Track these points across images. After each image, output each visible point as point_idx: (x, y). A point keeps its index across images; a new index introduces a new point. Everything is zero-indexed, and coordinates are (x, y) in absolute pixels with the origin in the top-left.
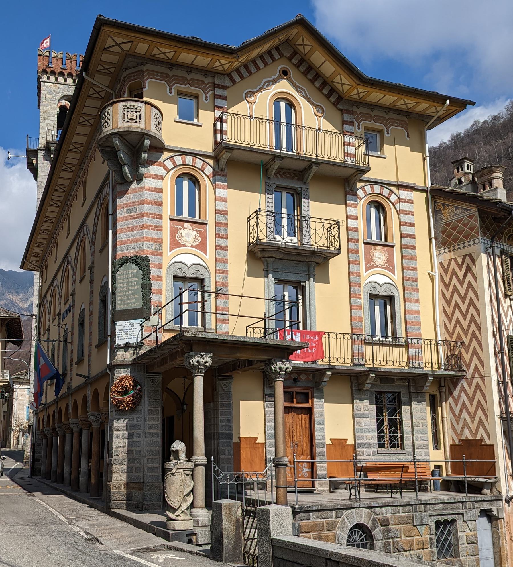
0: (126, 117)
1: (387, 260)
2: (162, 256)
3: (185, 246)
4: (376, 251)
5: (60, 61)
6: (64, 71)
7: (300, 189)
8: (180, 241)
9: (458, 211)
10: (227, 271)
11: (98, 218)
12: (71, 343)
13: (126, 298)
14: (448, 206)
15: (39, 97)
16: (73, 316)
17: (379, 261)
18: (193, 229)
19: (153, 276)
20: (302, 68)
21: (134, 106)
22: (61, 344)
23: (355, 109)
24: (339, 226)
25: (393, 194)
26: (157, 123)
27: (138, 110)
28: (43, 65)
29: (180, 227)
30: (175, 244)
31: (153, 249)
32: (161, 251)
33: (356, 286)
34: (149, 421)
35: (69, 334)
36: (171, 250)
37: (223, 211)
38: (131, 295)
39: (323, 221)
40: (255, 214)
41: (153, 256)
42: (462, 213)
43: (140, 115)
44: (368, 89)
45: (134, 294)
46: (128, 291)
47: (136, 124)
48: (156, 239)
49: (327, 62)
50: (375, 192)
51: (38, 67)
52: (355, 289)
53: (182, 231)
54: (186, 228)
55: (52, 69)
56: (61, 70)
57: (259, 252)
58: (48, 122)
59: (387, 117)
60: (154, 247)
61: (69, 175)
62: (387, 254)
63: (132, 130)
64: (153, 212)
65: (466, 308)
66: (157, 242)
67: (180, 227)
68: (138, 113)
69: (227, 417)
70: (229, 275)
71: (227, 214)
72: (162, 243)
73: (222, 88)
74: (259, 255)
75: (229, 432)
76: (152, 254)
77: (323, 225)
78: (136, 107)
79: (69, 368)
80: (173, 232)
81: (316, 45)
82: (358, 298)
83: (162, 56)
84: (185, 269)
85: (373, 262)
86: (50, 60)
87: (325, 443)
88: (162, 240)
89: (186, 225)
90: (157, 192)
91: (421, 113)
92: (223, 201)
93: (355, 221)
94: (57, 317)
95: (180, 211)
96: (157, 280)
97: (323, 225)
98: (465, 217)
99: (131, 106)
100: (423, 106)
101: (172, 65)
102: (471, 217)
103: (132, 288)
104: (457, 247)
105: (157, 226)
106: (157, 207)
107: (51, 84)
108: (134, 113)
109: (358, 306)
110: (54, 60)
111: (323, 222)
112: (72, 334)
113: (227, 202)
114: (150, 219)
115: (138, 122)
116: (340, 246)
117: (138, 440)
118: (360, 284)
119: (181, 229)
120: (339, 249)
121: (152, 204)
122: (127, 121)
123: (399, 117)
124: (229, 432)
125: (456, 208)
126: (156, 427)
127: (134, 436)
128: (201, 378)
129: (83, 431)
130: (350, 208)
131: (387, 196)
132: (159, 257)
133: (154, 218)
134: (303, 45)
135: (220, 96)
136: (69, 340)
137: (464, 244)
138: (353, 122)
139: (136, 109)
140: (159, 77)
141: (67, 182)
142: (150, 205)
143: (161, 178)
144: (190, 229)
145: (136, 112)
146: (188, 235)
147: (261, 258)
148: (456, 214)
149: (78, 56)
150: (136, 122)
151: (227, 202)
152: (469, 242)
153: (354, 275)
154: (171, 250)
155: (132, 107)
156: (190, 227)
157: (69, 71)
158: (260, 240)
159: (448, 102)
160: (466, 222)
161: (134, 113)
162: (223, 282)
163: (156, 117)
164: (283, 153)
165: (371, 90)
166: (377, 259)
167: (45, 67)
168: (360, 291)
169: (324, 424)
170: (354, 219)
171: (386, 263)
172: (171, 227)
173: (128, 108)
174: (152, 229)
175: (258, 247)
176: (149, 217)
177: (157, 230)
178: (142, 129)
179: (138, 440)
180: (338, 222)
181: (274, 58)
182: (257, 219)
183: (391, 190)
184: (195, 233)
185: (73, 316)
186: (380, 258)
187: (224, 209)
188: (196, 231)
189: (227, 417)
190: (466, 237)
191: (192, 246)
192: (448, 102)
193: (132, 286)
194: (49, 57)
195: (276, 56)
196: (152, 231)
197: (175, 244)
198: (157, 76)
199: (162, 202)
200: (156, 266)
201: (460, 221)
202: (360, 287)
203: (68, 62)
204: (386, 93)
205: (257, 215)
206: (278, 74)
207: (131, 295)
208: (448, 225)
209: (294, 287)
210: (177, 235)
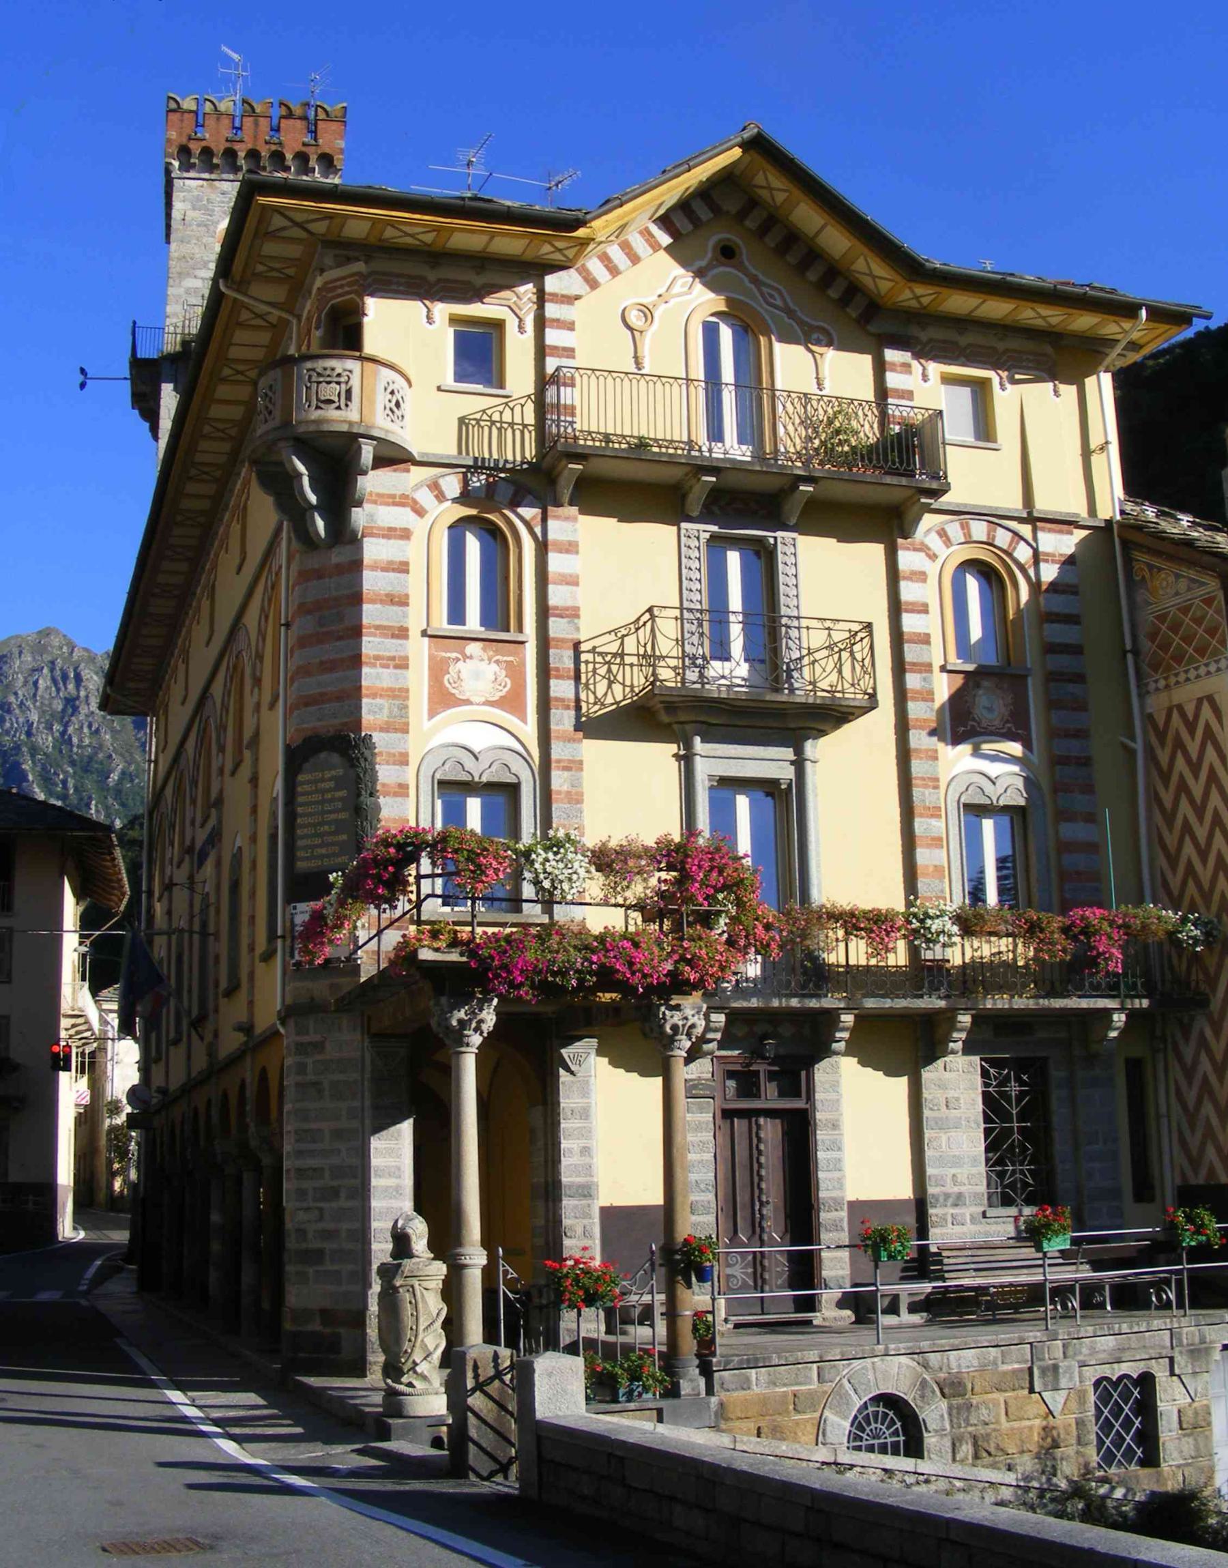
0: (314, 398)
1: (1012, 714)
2: (407, 732)
3: (468, 702)
4: (981, 692)
5: (226, 122)
6: (237, 147)
7: (772, 541)
8: (454, 691)
9: (1183, 585)
10: (581, 762)
11: (267, 617)
12: (217, 938)
13: (318, 841)
14: (1160, 569)
15: (168, 216)
16: (218, 864)
17: (990, 716)
18: (490, 660)
19: (384, 785)
20: (771, 240)
21: (333, 369)
22: (196, 937)
23: (914, 331)
24: (871, 635)
25: (1022, 543)
26: (393, 405)
27: (342, 379)
28: (180, 134)
29: (454, 655)
30: (443, 699)
31: (383, 717)
32: (403, 720)
33: (926, 786)
34: (758, 1072)
35: (212, 910)
36: (432, 714)
37: (567, 609)
38: (330, 834)
39: (828, 624)
40: (647, 616)
41: (383, 735)
42: (1189, 589)
43: (349, 392)
44: (938, 289)
45: (336, 833)
46: (322, 824)
47: (338, 413)
48: (392, 690)
49: (829, 228)
50: (975, 539)
51: (169, 141)
52: (923, 794)
53: (460, 664)
54: (471, 657)
55: (204, 144)
56: (228, 145)
57: (662, 712)
58: (190, 283)
59: (1001, 346)
60: (386, 711)
61: (210, 489)
62: (1009, 699)
63: (326, 427)
64: (385, 623)
65: (1206, 834)
66: (394, 697)
67: (454, 655)
68: (343, 386)
69: (582, 1143)
70: (585, 774)
71: (578, 616)
72: (407, 698)
73: (562, 302)
74: (665, 719)
75: (588, 1179)
76: (382, 730)
77: (829, 635)
78: (339, 370)
79: (211, 1005)
80: (438, 670)
81: (797, 193)
82: (932, 816)
83: (409, 240)
84: (469, 763)
85: (974, 720)
86: (200, 120)
87: (843, 1199)
88: (407, 690)
89: (473, 648)
90: (394, 570)
91: (1088, 334)
92: (568, 584)
93: (923, 616)
94: (187, 858)
95: (457, 613)
96: (396, 795)
97: (829, 635)
98: (1197, 601)
99: (325, 369)
100: (1084, 322)
101: (437, 256)
102: (1208, 601)
103: (333, 816)
104: (1162, 683)
105: (393, 659)
106: (395, 608)
107: (200, 182)
108: (333, 385)
109: (933, 839)
110: (210, 122)
111: (829, 629)
112: (218, 912)
113: (576, 584)
114: (377, 640)
115: (343, 406)
116: (874, 689)
117: (350, 1204)
118: (937, 780)
119: (458, 660)
120: (873, 696)
121: (382, 602)
122: (318, 407)
123: (1030, 345)
124: (588, 1179)
125: (1177, 576)
126: (382, 1173)
127: (343, 1195)
128: (473, 1056)
129: (245, 1176)
130: (910, 583)
131: (1005, 547)
132: (399, 735)
133: (385, 636)
134: (770, 189)
135: (558, 320)
136: (211, 929)
137: (1196, 669)
138: (909, 366)
139: (339, 375)
140: (401, 288)
141: (205, 505)
142: (378, 606)
143: (405, 534)
144: (482, 660)
145: (338, 383)
146: (477, 675)
147: (670, 725)
148: (1177, 594)
149: (276, 105)
150: (339, 408)
151: (576, 584)
152: (1207, 665)
153: (921, 758)
154: (432, 714)
155: (328, 372)
156: (481, 653)
157: (250, 146)
158: (661, 681)
159: (1144, 313)
160: (1199, 614)
161: (333, 385)
162: (568, 793)
163: (389, 390)
164: (717, 459)
165: (945, 291)
166: (985, 712)
167: (184, 141)
168: (938, 799)
169: (839, 1149)
170: (919, 612)
171: (1007, 721)
172: (432, 658)
173: (319, 375)
174: (383, 666)
175: (658, 699)
176: (375, 635)
177: (396, 667)
178: (351, 423)
179: (350, 1204)
180: (869, 627)
181: (699, 219)
182: (653, 630)
183: (1015, 533)
184: (494, 667)
185: (218, 864)
186: (990, 710)
187: (570, 603)
188: (497, 662)
189: (582, 1143)
190: (1201, 651)
191: (488, 703)
192: (1144, 313)
193: (330, 812)
194: (196, 113)
195: (704, 213)
196: (381, 670)
197: (443, 699)
198: (399, 284)
199: (407, 596)
200: (391, 759)
201: (1185, 610)
202: (936, 787)
203: (248, 122)
204: (986, 297)
205: (653, 617)
206: (710, 255)
207: (330, 834)
208: (1162, 618)
209: (768, 794)
210: (447, 677)
